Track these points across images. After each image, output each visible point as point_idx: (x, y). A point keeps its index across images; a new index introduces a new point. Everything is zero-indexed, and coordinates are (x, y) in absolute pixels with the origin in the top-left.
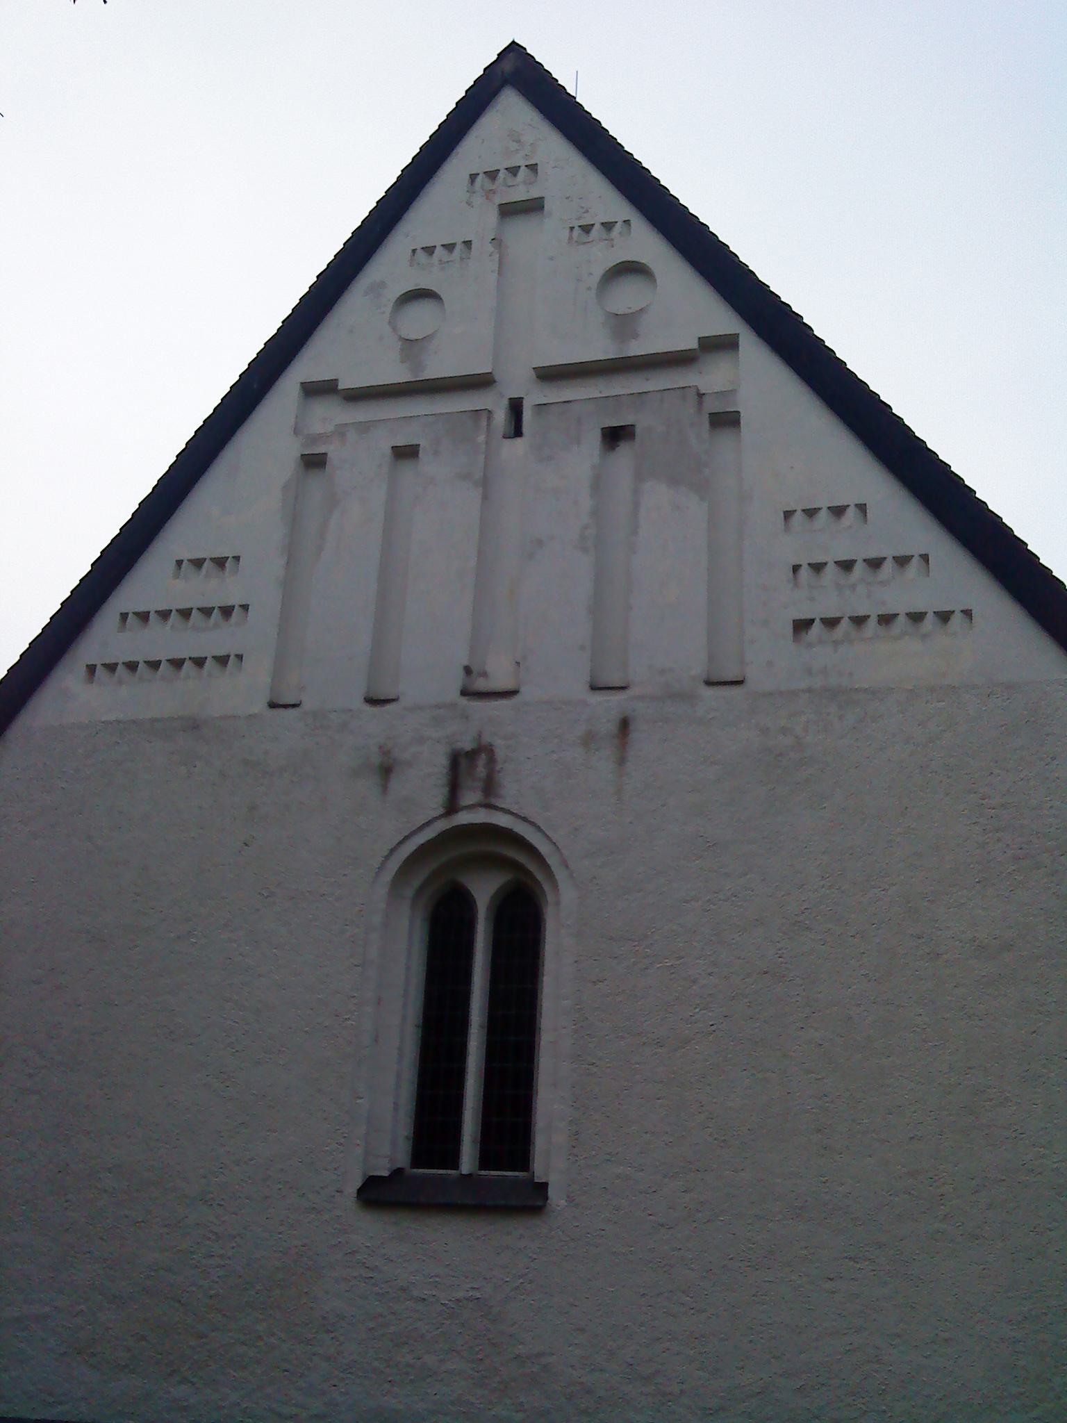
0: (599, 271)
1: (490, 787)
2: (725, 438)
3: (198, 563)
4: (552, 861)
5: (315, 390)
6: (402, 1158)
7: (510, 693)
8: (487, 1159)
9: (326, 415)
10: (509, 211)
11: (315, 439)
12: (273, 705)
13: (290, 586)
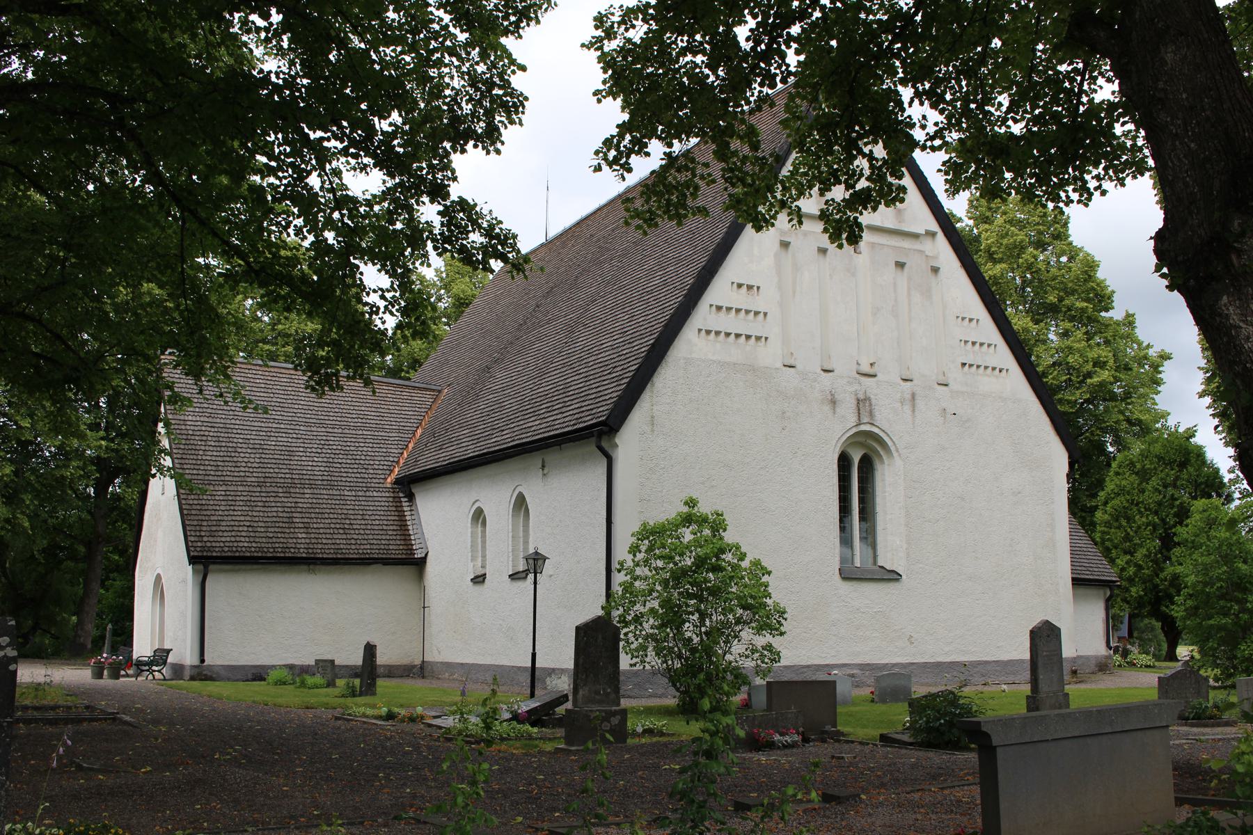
1: (871, 414)
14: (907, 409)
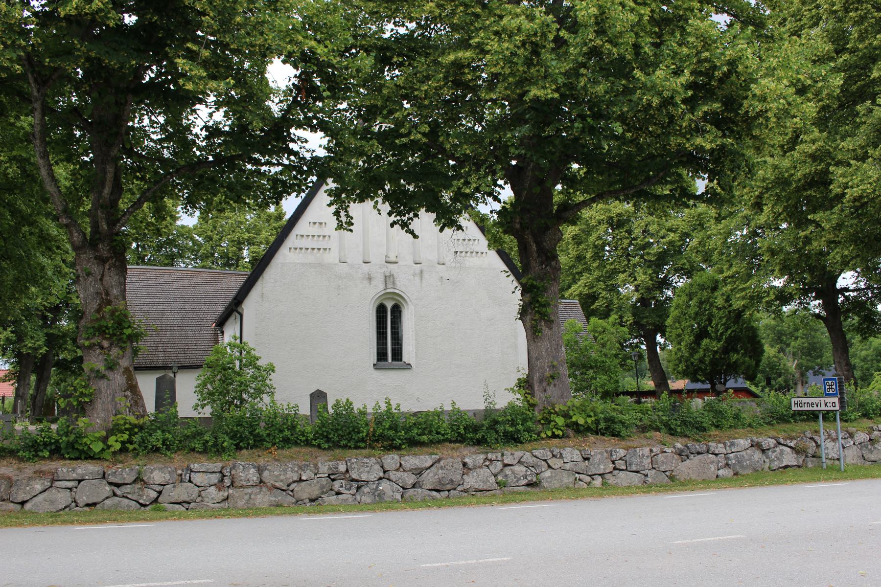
1: (394, 283)
3: (315, 223)
4: (408, 300)
8: (393, 359)
14: (417, 279)
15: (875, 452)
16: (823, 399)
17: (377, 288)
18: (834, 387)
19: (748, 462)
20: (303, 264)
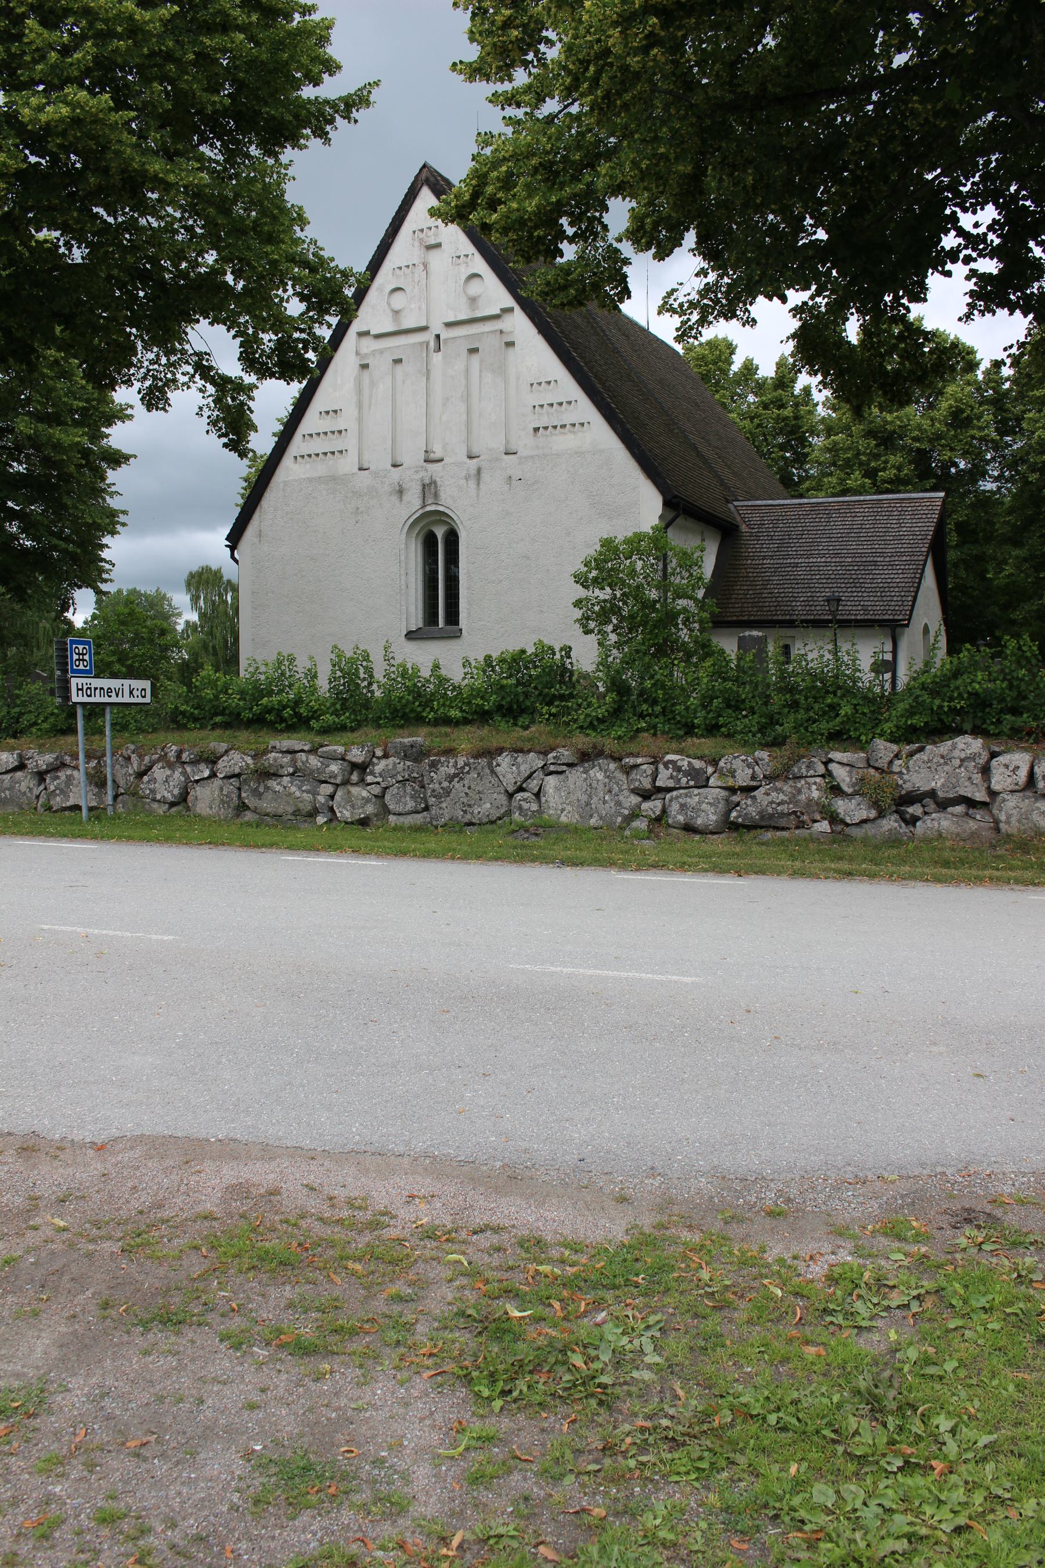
0: (464, 277)
1: (436, 495)
2: (511, 350)
3: (327, 413)
5: (362, 334)
6: (421, 625)
7: (442, 460)
9: (368, 345)
10: (429, 248)
11: (366, 355)
12: (360, 469)
13: (360, 420)
14: (472, 484)
15: (269, 795)
16: (127, 682)
17: (413, 504)
18: (86, 657)
19: (7, 793)
20: (310, 480)
